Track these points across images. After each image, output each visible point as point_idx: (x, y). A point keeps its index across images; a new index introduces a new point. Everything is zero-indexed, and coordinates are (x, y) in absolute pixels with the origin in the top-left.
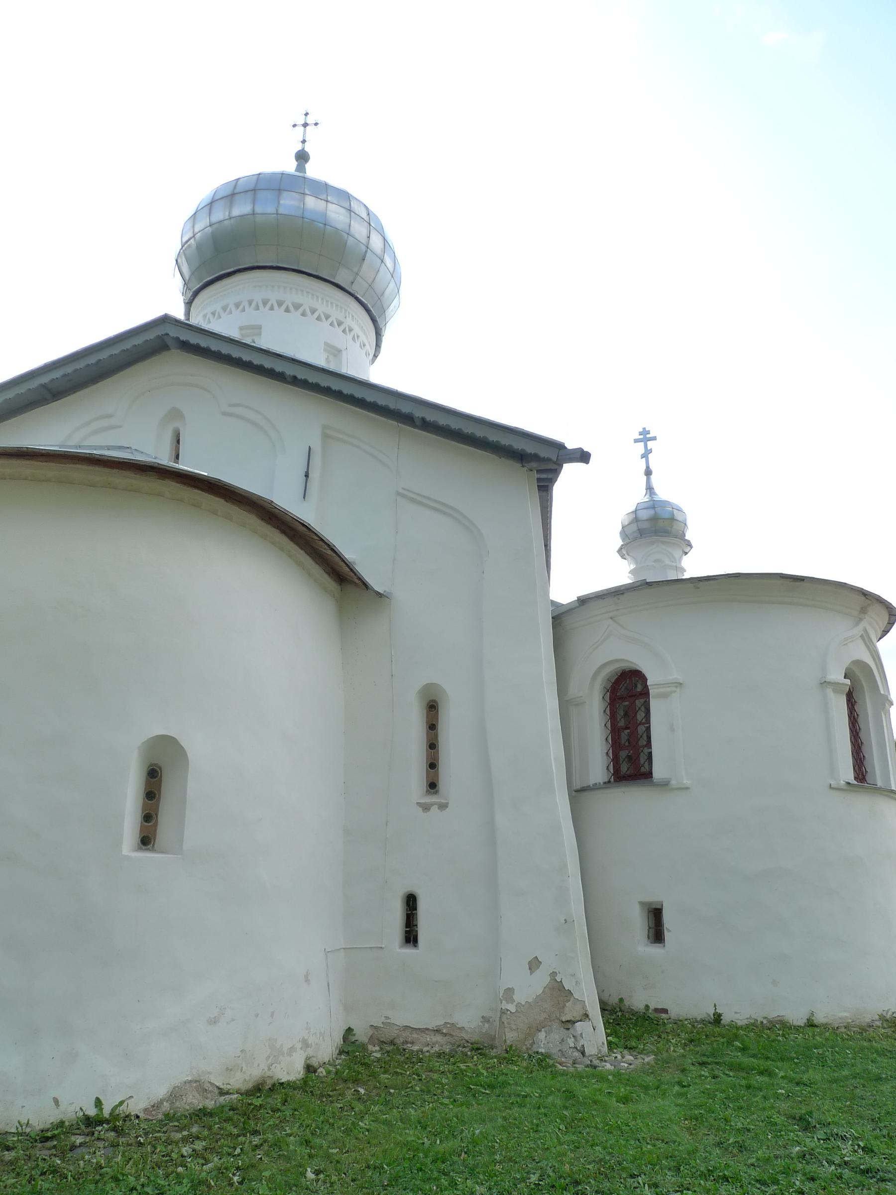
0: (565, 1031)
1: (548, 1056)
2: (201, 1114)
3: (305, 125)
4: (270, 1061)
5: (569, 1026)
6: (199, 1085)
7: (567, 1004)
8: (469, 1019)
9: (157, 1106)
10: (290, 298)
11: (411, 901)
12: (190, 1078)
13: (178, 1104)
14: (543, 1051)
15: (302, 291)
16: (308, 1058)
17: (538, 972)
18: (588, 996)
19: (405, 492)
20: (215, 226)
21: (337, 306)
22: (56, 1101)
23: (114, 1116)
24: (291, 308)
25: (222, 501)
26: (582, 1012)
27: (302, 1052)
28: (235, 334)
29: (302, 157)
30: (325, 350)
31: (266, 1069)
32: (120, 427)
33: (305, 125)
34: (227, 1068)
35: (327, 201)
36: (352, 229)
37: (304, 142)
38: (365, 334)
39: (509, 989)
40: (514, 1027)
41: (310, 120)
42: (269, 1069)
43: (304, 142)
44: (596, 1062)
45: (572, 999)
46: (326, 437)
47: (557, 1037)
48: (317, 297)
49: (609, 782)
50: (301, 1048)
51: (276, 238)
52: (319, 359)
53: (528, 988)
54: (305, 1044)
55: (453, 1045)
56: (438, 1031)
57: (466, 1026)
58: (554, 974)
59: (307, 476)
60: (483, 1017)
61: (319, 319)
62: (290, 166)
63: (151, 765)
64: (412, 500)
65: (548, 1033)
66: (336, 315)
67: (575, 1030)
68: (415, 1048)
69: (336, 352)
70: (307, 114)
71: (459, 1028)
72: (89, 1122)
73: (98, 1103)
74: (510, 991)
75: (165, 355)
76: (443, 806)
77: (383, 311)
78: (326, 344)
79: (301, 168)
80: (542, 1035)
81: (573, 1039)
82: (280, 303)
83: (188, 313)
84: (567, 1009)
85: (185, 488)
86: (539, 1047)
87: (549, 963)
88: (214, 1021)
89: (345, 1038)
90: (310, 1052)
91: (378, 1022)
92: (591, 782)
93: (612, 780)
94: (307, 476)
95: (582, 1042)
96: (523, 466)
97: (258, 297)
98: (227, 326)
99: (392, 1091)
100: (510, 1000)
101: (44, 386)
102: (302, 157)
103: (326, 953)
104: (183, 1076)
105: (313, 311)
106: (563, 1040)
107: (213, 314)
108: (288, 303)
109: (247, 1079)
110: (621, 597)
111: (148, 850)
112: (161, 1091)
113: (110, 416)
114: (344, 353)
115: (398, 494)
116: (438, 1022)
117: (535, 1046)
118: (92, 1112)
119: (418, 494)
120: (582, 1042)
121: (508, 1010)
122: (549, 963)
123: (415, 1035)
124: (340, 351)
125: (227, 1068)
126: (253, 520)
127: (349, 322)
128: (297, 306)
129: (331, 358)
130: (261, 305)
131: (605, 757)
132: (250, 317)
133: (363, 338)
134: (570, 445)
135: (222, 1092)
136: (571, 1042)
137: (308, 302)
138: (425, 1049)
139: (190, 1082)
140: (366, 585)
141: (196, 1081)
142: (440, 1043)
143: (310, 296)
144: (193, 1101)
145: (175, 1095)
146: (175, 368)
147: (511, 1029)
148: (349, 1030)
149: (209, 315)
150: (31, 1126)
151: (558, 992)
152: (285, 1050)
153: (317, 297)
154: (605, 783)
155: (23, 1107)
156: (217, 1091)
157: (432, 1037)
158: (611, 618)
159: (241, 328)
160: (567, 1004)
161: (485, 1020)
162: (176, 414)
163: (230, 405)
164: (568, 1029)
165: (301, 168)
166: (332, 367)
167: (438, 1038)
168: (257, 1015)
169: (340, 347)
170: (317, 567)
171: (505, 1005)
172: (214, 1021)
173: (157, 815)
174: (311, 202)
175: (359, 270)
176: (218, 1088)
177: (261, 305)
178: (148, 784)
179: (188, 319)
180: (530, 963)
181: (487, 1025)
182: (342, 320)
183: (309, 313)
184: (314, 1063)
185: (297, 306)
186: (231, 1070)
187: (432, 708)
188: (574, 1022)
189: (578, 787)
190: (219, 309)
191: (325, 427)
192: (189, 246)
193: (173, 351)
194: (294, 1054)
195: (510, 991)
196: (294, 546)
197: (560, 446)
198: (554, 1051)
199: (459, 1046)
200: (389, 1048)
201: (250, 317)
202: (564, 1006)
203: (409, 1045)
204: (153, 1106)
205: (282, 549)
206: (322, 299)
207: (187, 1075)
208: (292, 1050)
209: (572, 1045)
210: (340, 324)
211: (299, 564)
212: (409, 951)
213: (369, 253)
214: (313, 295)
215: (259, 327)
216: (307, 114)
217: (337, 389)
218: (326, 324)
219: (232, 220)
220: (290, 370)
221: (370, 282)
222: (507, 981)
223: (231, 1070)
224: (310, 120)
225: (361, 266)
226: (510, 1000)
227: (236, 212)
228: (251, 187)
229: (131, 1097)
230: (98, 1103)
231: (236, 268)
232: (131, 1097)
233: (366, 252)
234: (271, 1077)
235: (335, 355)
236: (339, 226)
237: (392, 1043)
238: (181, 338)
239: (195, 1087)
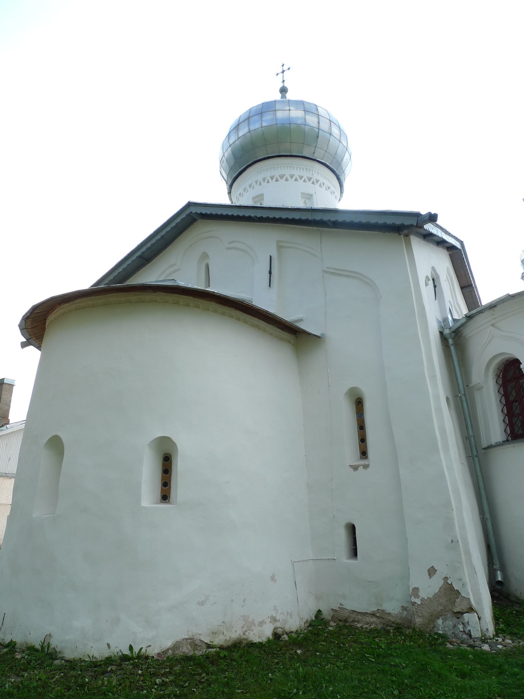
0: (457, 620)
1: (443, 637)
2: (187, 659)
3: (283, 72)
4: (244, 629)
5: (460, 616)
6: (193, 642)
7: (457, 600)
8: (393, 607)
9: (165, 652)
10: (276, 173)
11: (352, 529)
12: (187, 637)
13: (177, 652)
14: (441, 632)
15: (284, 167)
16: (276, 628)
17: (435, 577)
18: (474, 595)
19: (327, 270)
20: (232, 146)
21: (306, 169)
22: (108, 645)
23: (139, 657)
24: (279, 178)
25: (192, 298)
26: (468, 606)
27: (271, 624)
28: (250, 203)
29: (283, 90)
30: (302, 197)
31: (242, 634)
32: (179, 270)
33: (283, 72)
34: (213, 633)
35: (290, 110)
36: (307, 121)
37: (283, 81)
38: (329, 181)
39: (415, 588)
40: (420, 614)
41: (285, 68)
42: (244, 634)
43: (283, 81)
44: (478, 643)
45: (460, 597)
46: (280, 247)
47: (451, 623)
48: (294, 168)
49: (507, 440)
50: (270, 622)
51: (271, 140)
52: (300, 204)
53: (429, 588)
54: (274, 619)
55: (384, 624)
56: (373, 615)
57: (392, 612)
58: (446, 579)
59: (270, 273)
60: (402, 606)
61: (296, 180)
62: (278, 96)
63: (165, 454)
64: (333, 273)
65: (444, 620)
66: (306, 174)
67: (463, 619)
68: (359, 625)
69: (309, 197)
70: (283, 65)
71: (387, 614)
72: (124, 658)
73: (131, 648)
74: (416, 590)
75: (195, 224)
76: (366, 467)
77: (339, 164)
78: (302, 194)
79: (284, 96)
80: (440, 621)
81: (462, 626)
82: (272, 178)
83: (231, 199)
84: (457, 604)
85: (168, 294)
86: (439, 629)
87: (442, 571)
88: (201, 604)
89: (316, 616)
90: (278, 624)
91: (336, 607)
92: (493, 441)
93: (510, 438)
94: (270, 273)
95: (469, 628)
96: (400, 235)
97: (260, 178)
98: (246, 200)
99: (318, 654)
100: (417, 596)
101: (140, 256)
102: (283, 90)
103: (293, 563)
104: (181, 635)
105: (301, 178)
106: (455, 626)
107: (240, 195)
108: (296, 176)
109: (228, 639)
110: (495, 309)
111: (166, 503)
112: (168, 644)
113: (174, 265)
114: (314, 196)
115: (324, 271)
116: (373, 609)
117: (435, 629)
118: (127, 652)
119: (336, 269)
120: (469, 628)
121: (415, 603)
122: (442, 571)
123: (359, 617)
124: (311, 195)
125: (213, 633)
126: (213, 305)
127: (315, 177)
128: (282, 177)
129: (307, 201)
130: (262, 182)
131: (503, 424)
132: (257, 190)
133: (327, 183)
134: (423, 212)
135: (209, 646)
136: (461, 627)
137: (287, 172)
138: (365, 626)
139: (187, 639)
140: (309, 334)
141: (191, 639)
142: (375, 623)
143: (289, 168)
144: (187, 650)
145: (176, 646)
146: (201, 231)
147: (419, 617)
148: (319, 611)
149: (238, 196)
150: (95, 658)
151: (450, 592)
152: (256, 622)
153: (294, 168)
154: (504, 441)
155: (92, 647)
156: (204, 646)
157: (370, 618)
158: (492, 325)
159: (253, 198)
160: (457, 600)
161: (404, 608)
162: (205, 256)
163: (229, 243)
164: (459, 618)
165: (284, 96)
166: (308, 206)
167: (374, 619)
168: (232, 601)
169: (311, 193)
170: (271, 326)
171: (413, 600)
172: (201, 604)
173: (170, 482)
174: (280, 115)
175: (316, 145)
176: (206, 644)
177: (262, 182)
178: (164, 465)
179: (232, 202)
180: (429, 570)
181: (405, 612)
182: (310, 176)
183: (289, 178)
184: (279, 631)
185: (282, 177)
186: (216, 633)
187: (359, 404)
188: (463, 613)
189: (486, 446)
190: (242, 191)
191: (278, 242)
192: (223, 161)
193: (199, 221)
194: (264, 626)
195: (416, 590)
196: (248, 316)
197: (417, 215)
198: (449, 633)
199: (387, 626)
200: (341, 624)
201: (257, 190)
202: (455, 602)
203: (356, 623)
204: (163, 652)
205: (239, 319)
206: (297, 168)
207: (185, 635)
208: (261, 623)
209: (462, 629)
210: (310, 179)
211: (253, 325)
212: (352, 561)
213: (321, 132)
214: (291, 167)
215: (262, 195)
216: (283, 65)
217: (279, 217)
218: (301, 182)
219: (240, 139)
220: (284, 215)
221: (325, 149)
222: (413, 584)
223: (216, 633)
224: (285, 68)
225: (317, 142)
226: (417, 596)
227: (241, 134)
228: (247, 117)
229: (150, 646)
230: (131, 648)
231: (244, 167)
232: (150, 646)
233: (319, 132)
234: (246, 639)
235: (309, 199)
236: (299, 122)
237: (346, 621)
238: (258, 216)
239: (190, 643)
